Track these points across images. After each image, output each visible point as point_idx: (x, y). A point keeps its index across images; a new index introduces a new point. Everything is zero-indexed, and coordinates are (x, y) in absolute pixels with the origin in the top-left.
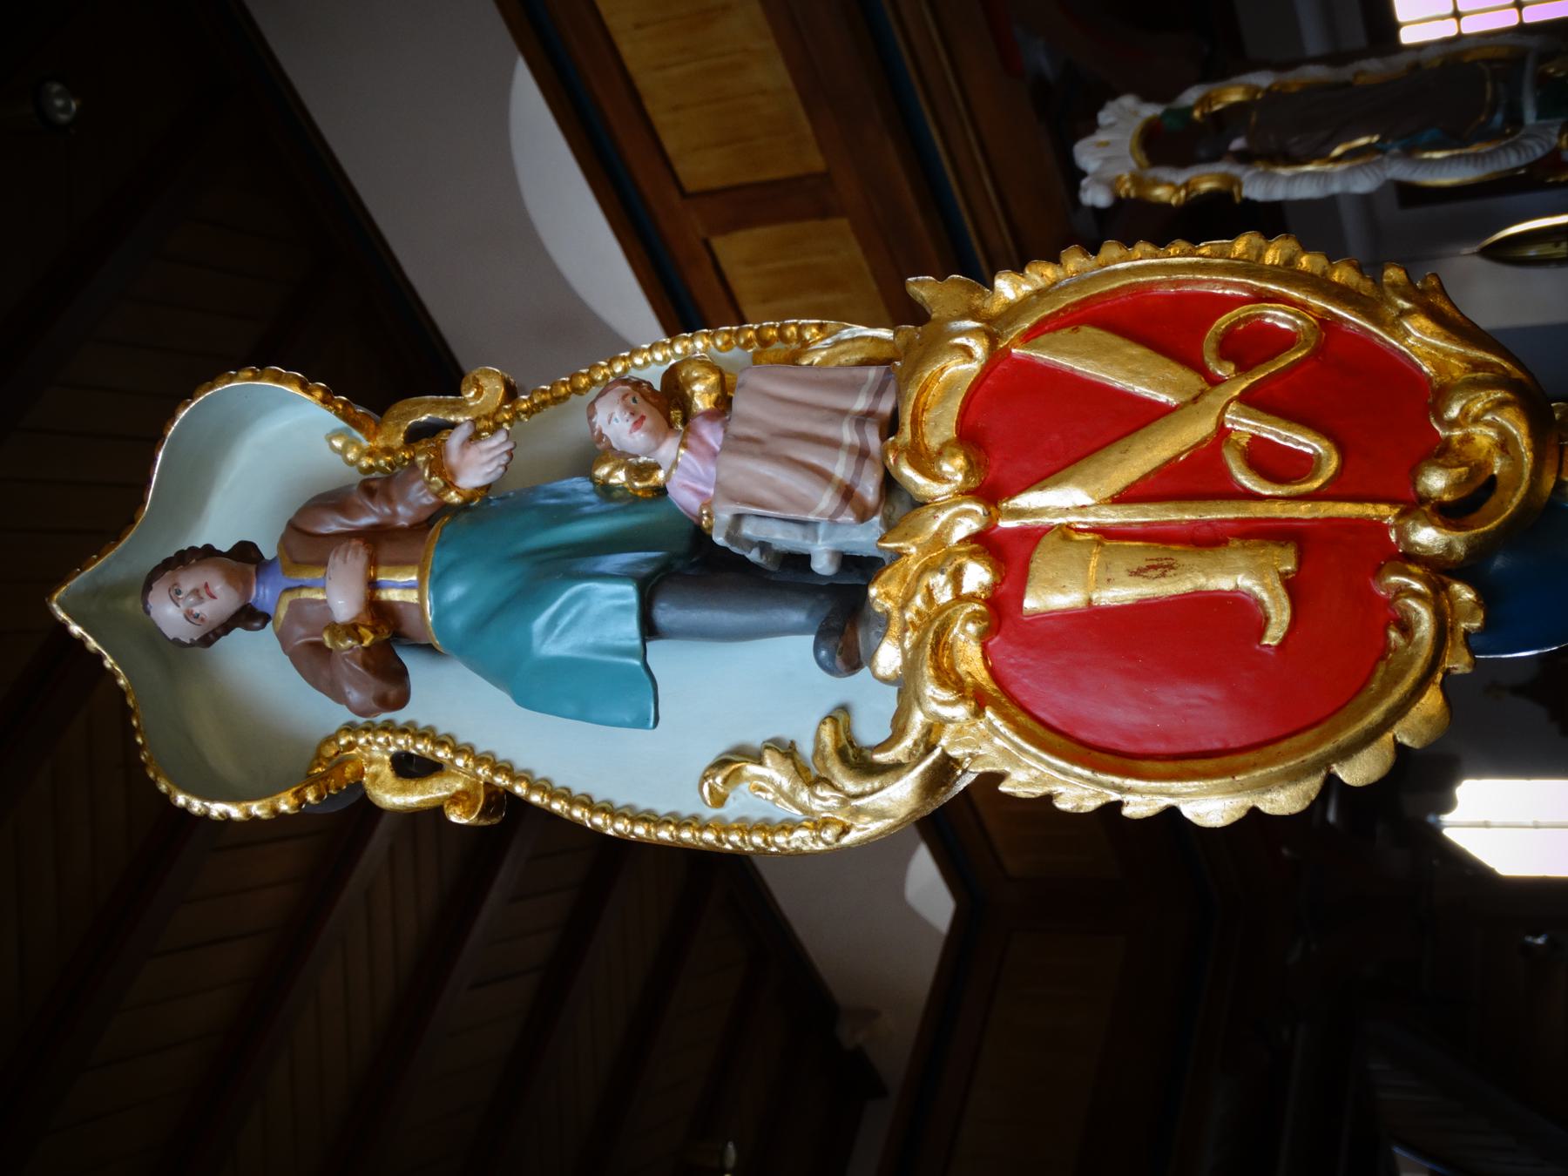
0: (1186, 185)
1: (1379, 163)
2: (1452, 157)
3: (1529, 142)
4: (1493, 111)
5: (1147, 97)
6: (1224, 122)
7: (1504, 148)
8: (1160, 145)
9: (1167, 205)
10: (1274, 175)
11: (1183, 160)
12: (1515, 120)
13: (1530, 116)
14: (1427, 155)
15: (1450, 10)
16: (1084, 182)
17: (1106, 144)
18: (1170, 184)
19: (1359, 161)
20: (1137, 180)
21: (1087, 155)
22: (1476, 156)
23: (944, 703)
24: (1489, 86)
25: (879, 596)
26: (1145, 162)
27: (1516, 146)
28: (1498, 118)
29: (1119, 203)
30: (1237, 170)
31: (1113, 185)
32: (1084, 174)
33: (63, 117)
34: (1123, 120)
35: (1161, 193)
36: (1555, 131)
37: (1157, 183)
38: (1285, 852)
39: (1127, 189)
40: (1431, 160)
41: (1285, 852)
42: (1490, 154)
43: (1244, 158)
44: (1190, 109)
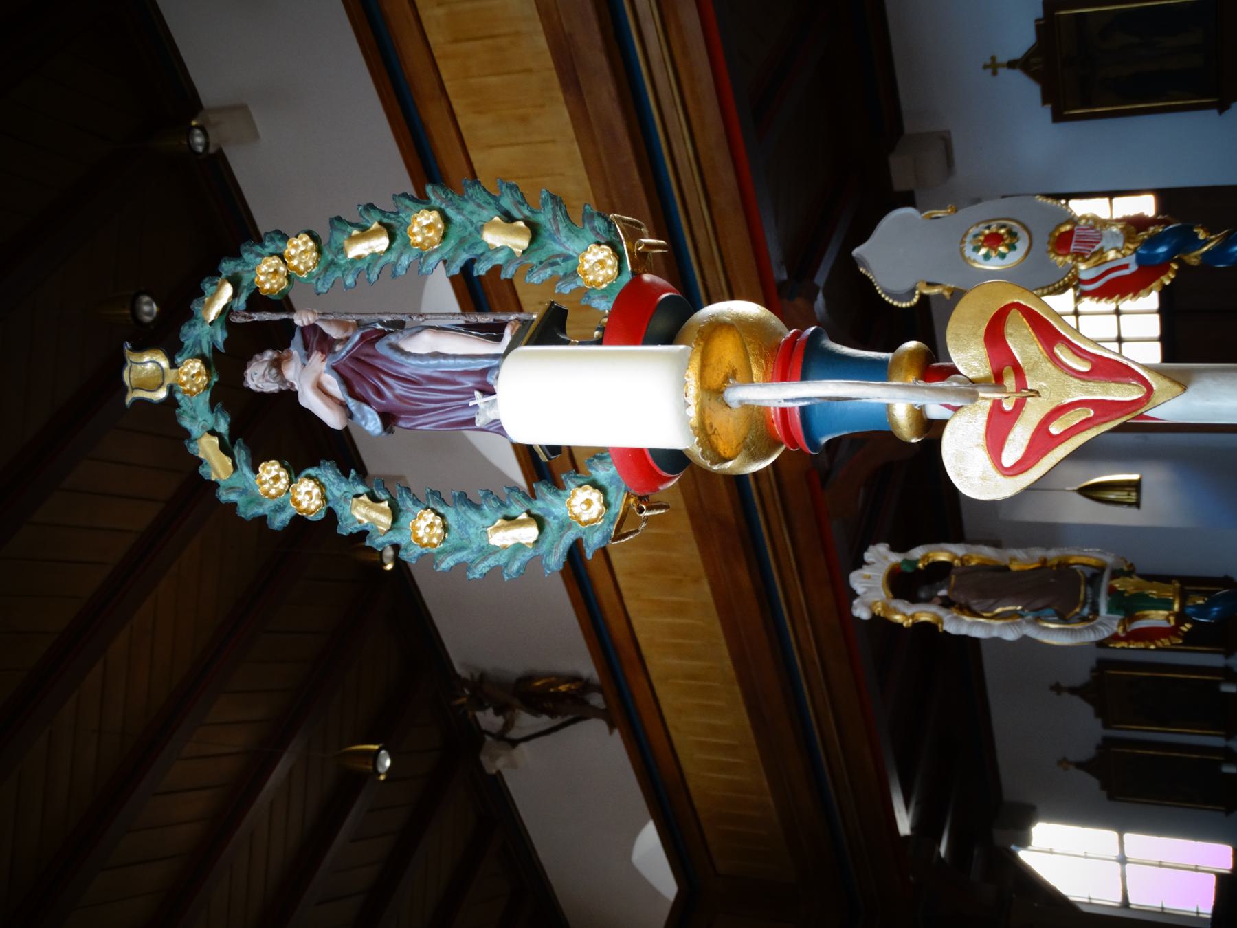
0: (912, 616)
1: (1018, 624)
2: (1059, 629)
3: (1101, 627)
4: (1083, 607)
5: (894, 549)
6: (940, 571)
7: (1087, 628)
8: (904, 584)
9: (901, 625)
10: (962, 620)
11: (914, 599)
12: (1095, 611)
13: (1103, 610)
14: (1046, 625)
15: (1115, 335)
16: (855, 602)
17: (869, 577)
18: (904, 614)
19: (1009, 621)
20: (886, 607)
21: (858, 581)
22: (1072, 631)
23: (320, 388)
24: (1082, 588)
25: (196, 127)
26: (891, 595)
27: (1093, 628)
28: (1086, 611)
29: (875, 618)
30: (942, 612)
31: (870, 607)
32: (855, 595)
33: (148, 319)
34: (881, 558)
35: (898, 618)
36: (1116, 623)
37: (897, 612)
38: (911, 878)
39: (878, 609)
40: (1047, 628)
41: (911, 878)
42: (1080, 631)
43: (947, 603)
44: (917, 561)
